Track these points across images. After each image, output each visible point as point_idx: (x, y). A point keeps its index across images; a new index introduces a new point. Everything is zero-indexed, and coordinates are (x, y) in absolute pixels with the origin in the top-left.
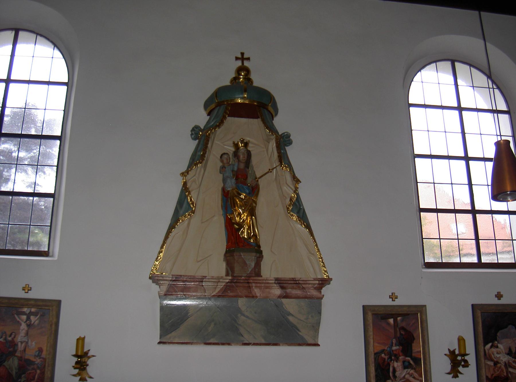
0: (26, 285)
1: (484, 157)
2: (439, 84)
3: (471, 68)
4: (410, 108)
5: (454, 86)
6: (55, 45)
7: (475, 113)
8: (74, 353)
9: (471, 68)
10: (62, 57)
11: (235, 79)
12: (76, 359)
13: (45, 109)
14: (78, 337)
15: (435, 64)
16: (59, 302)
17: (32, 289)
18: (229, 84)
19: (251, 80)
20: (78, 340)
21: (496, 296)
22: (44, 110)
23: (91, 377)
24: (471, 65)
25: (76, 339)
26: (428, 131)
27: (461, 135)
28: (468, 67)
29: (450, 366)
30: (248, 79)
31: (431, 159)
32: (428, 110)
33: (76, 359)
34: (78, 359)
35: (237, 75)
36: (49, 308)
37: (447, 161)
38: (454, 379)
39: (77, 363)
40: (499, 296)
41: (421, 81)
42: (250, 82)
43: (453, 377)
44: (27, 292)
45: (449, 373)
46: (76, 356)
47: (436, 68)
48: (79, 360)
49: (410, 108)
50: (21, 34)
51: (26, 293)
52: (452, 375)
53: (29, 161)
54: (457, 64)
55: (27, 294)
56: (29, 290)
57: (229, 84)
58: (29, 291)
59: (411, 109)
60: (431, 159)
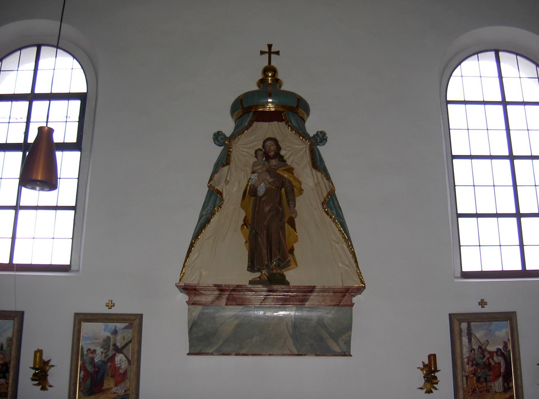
0: (109, 300)
1: (471, 155)
2: (520, 78)
3: (518, 57)
4: (449, 105)
5: (498, 79)
6: (74, 57)
7: (522, 107)
8: (32, 366)
9: (518, 57)
10: (81, 68)
11: (262, 82)
12: (33, 371)
13: (487, 130)
14: (36, 349)
15: (477, 55)
16: (141, 316)
17: (115, 305)
18: (256, 88)
19: (280, 81)
20: (36, 352)
21: (479, 304)
22: (65, 123)
23: (51, 386)
24: (517, 54)
25: (34, 351)
26: (528, 130)
27: (505, 132)
28: (515, 56)
29: (424, 380)
30: (277, 81)
31: (532, 160)
32: (527, 107)
33: (33, 371)
34: (36, 372)
35: (264, 76)
36: (132, 322)
37: (489, 161)
38: (42, 391)
39: (35, 375)
40: (482, 303)
41: (461, 76)
42: (278, 84)
43: (426, 392)
44: (111, 308)
45: (421, 388)
46: (34, 368)
47: (55, 53)
48: (37, 372)
49: (449, 105)
50: (43, 49)
51: (109, 308)
52: (40, 387)
53: (256, 179)
54: (501, 54)
55: (110, 309)
56: (112, 306)
57: (256, 88)
58: (112, 307)
59: (449, 106)
60: (491, 160)
